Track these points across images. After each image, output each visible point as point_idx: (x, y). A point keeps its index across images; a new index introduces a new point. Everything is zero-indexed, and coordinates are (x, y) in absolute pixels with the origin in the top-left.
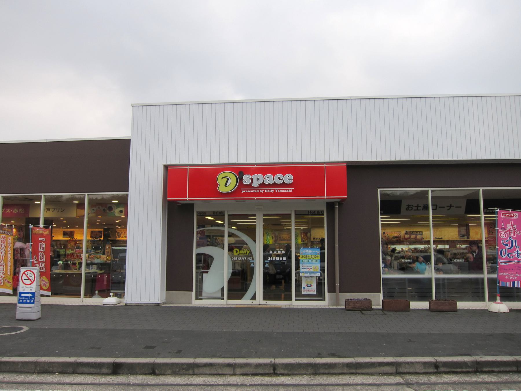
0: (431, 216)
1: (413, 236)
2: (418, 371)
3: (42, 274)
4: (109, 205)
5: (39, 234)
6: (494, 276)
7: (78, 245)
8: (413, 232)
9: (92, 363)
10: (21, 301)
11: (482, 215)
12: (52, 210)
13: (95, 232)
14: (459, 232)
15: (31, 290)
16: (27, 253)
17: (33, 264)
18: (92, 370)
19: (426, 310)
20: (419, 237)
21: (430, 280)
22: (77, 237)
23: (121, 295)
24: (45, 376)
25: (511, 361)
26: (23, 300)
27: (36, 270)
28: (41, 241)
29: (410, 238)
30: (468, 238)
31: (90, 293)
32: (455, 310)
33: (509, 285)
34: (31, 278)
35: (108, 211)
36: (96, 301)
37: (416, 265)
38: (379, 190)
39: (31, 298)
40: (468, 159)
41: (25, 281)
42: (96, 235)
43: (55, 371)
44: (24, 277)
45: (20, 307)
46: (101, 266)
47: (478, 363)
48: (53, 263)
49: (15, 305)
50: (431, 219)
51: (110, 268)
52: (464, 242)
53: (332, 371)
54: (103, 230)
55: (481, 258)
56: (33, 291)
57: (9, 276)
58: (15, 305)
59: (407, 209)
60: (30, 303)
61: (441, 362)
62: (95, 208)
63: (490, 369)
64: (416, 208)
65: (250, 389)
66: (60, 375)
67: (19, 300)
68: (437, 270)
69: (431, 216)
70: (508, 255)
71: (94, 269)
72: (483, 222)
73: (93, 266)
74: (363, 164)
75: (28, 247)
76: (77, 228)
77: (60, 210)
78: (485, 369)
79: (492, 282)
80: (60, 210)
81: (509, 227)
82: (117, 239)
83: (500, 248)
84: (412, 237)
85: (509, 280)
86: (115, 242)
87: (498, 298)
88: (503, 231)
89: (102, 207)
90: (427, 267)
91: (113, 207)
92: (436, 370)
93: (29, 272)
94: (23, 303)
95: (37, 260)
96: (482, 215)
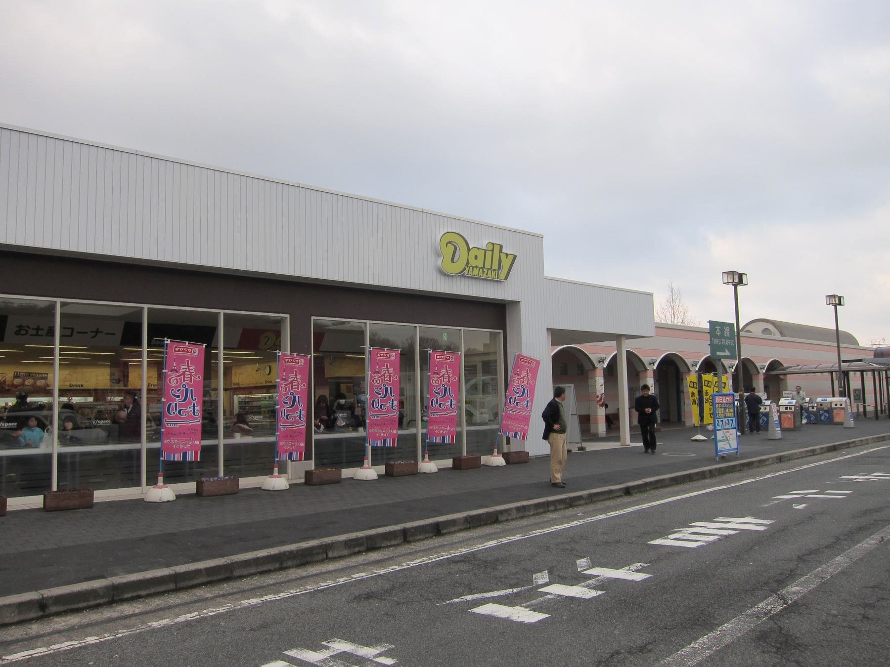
0: (57, 346)
1: (29, 382)
2: (7, 620)
6: (157, 445)
8: (29, 374)
11: (145, 349)
14: (112, 374)
18: (606, 496)
19: (38, 510)
20: (40, 383)
21: (49, 457)
25: (166, 576)
29: (23, 384)
30: (126, 385)
32: (89, 505)
33: (178, 457)
37: (25, 432)
38: (313, 318)
40: (129, 256)
47: (115, 588)
50: (57, 352)
52: (119, 392)
53: (613, 495)
55: (139, 417)
59: (17, 333)
61: (51, 597)
63: (135, 594)
64: (34, 332)
68: (64, 440)
69: (57, 346)
70: (179, 412)
72: (145, 359)
74: (15, 250)
78: (126, 596)
79: (154, 454)
81: (183, 367)
83: (168, 401)
84: (27, 383)
85: (178, 451)
87: (161, 479)
88: (436, 376)
90: (46, 435)
92: (41, 614)
96: (145, 349)
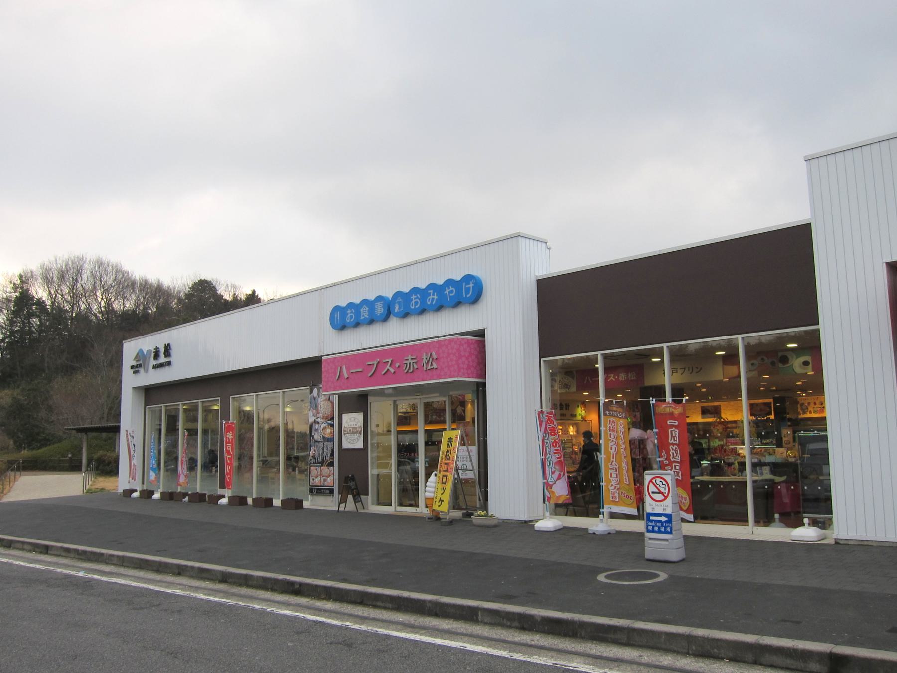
3: (678, 483)
4: (780, 354)
5: (666, 414)
7: (730, 430)
9: (789, 648)
10: (650, 528)
12: (680, 371)
13: (757, 405)
15: (665, 510)
16: (650, 447)
17: (662, 466)
22: (728, 415)
23: (824, 523)
24: (707, 661)
26: (653, 527)
27: (669, 476)
28: (672, 426)
31: (765, 519)
34: (662, 489)
35: (781, 365)
36: (776, 533)
39: (666, 525)
41: (653, 495)
42: (761, 410)
43: (723, 655)
44: (652, 488)
45: (650, 539)
46: (776, 468)
48: (694, 463)
49: (642, 535)
51: (796, 471)
54: (771, 400)
56: (669, 512)
57: (627, 487)
58: (642, 534)
60: (666, 532)
62: (755, 362)
65: (644, 670)
66: (732, 663)
67: (647, 526)
71: (766, 474)
73: (764, 468)
75: (652, 438)
76: (724, 400)
77: (695, 370)
80: (695, 370)
82: (802, 416)
86: (797, 424)
89: (768, 357)
91: (789, 357)
93: (658, 480)
94: (653, 532)
95: (668, 458)
